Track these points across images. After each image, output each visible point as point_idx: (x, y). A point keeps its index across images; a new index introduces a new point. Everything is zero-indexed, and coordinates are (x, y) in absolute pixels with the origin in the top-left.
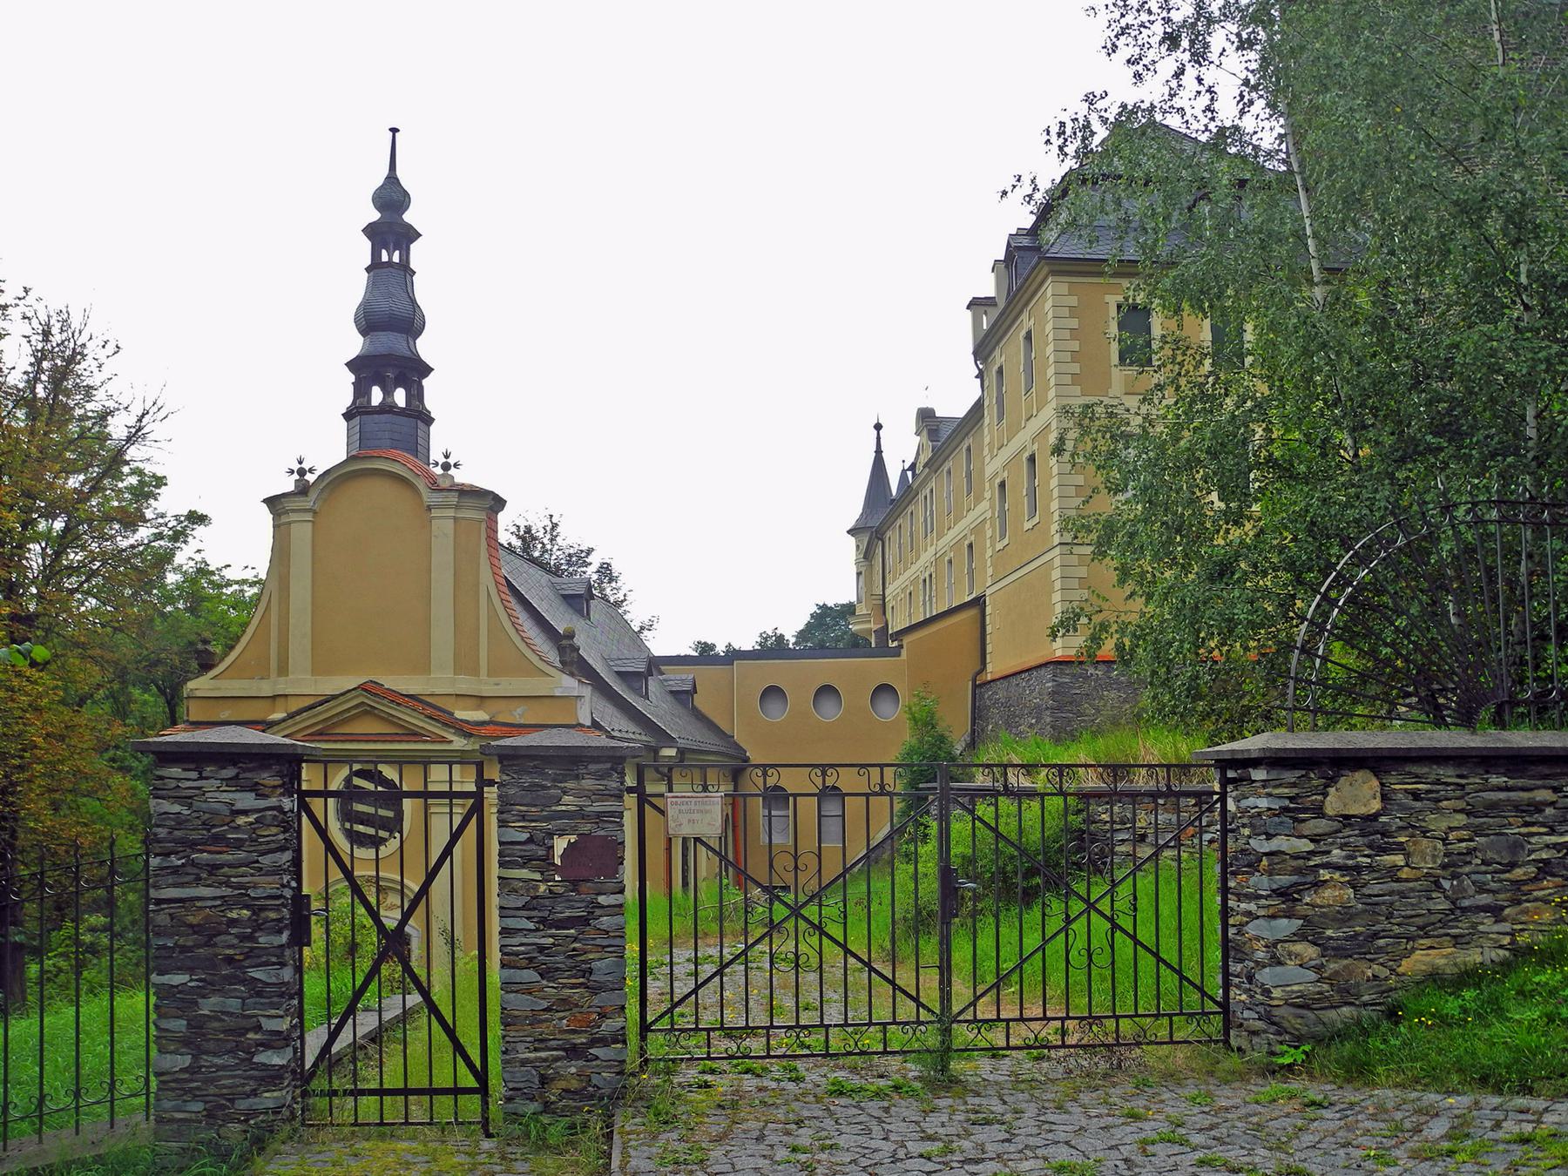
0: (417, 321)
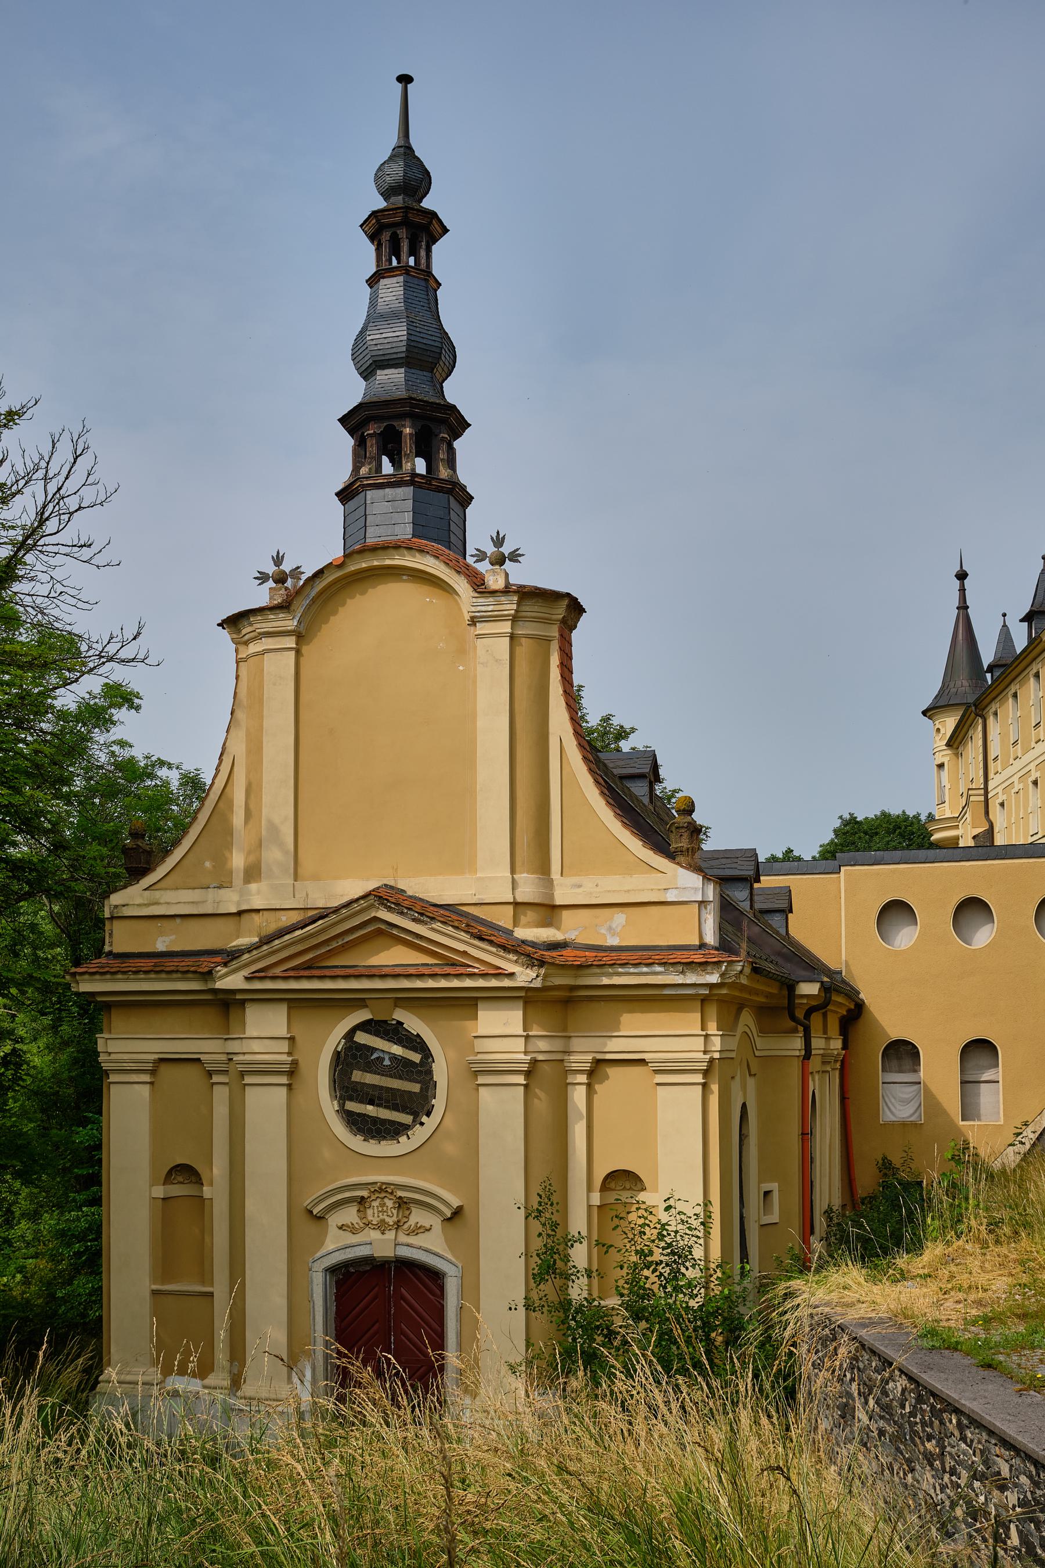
0: (445, 357)
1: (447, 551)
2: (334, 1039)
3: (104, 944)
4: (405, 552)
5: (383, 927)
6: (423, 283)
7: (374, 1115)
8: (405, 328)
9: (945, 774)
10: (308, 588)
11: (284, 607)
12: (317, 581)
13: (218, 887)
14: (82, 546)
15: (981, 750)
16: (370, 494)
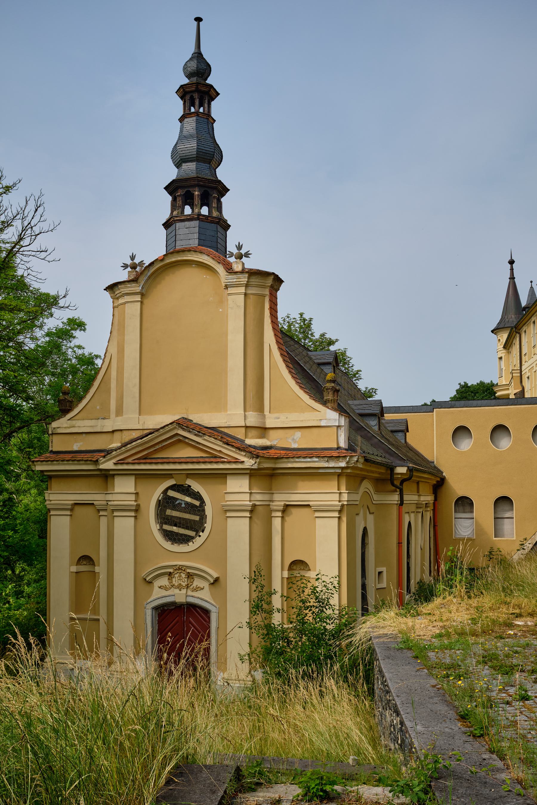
0: (216, 156)
1: (215, 252)
2: (157, 494)
3: (49, 447)
4: (193, 253)
5: (181, 438)
6: (206, 120)
7: (177, 532)
8: (196, 143)
9: (503, 362)
10: (146, 272)
11: (135, 280)
12: (151, 268)
13: (103, 419)
14: (41, 252)
15: (518, 350)
16: (178, 225)
